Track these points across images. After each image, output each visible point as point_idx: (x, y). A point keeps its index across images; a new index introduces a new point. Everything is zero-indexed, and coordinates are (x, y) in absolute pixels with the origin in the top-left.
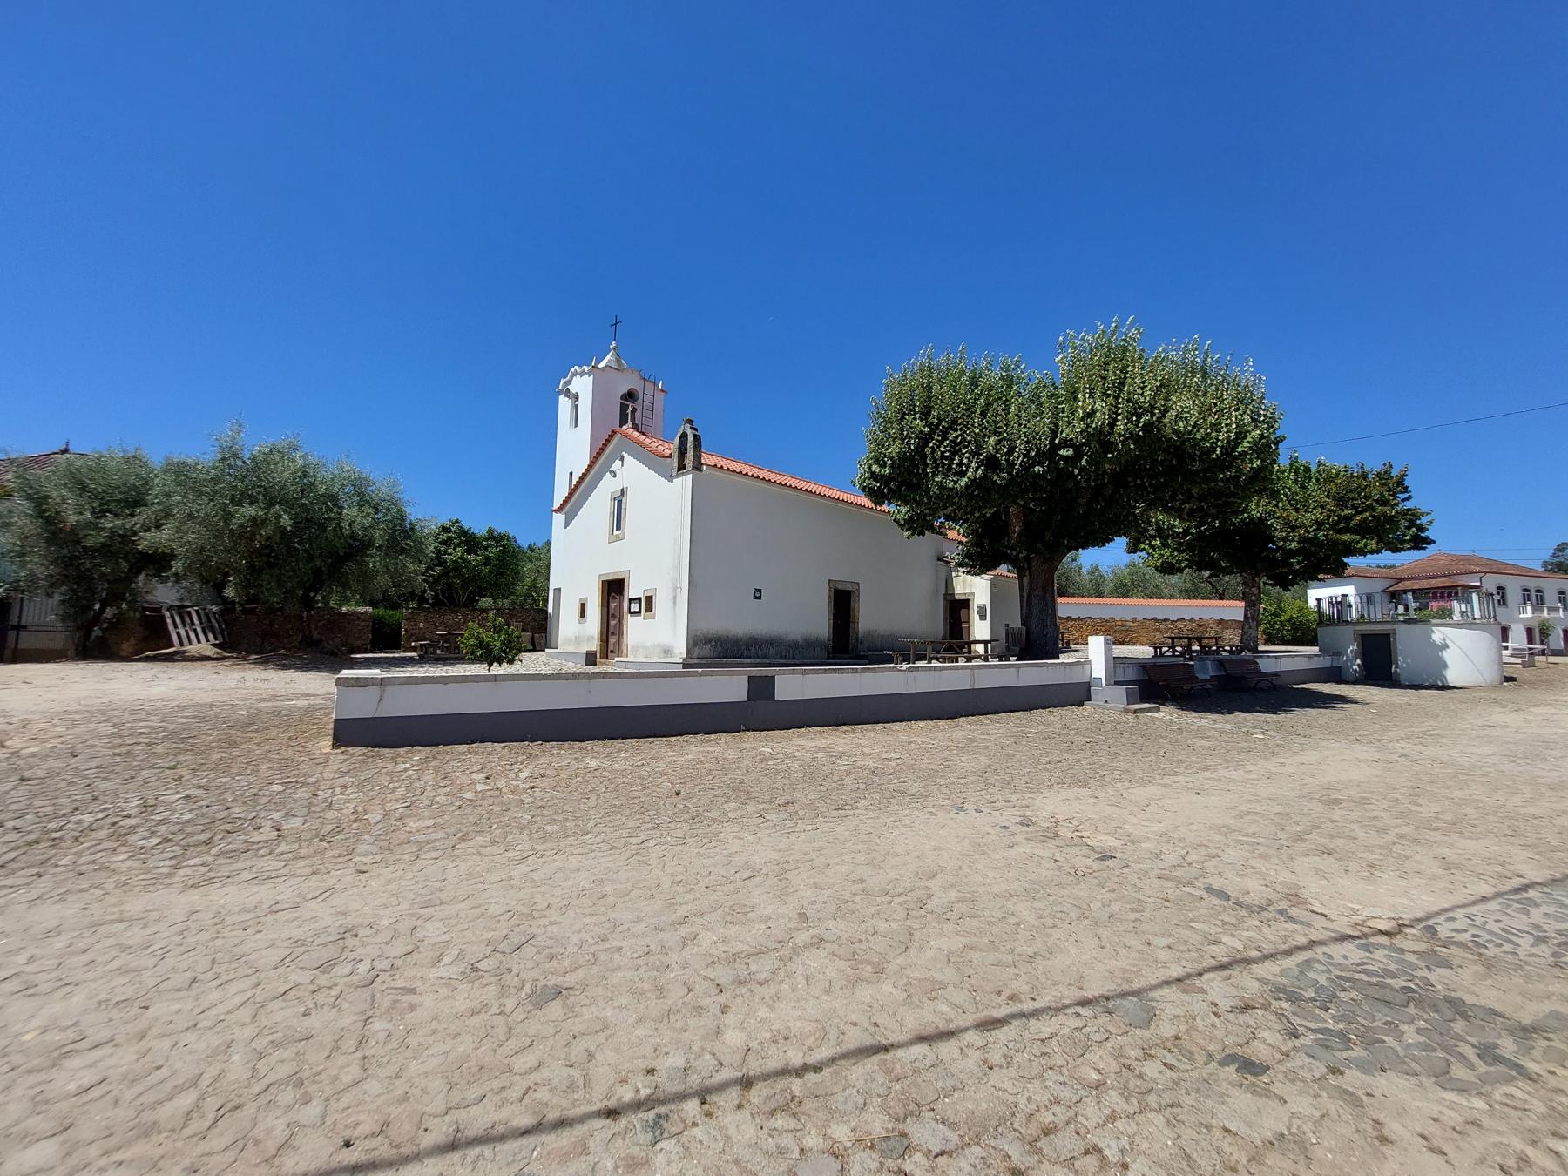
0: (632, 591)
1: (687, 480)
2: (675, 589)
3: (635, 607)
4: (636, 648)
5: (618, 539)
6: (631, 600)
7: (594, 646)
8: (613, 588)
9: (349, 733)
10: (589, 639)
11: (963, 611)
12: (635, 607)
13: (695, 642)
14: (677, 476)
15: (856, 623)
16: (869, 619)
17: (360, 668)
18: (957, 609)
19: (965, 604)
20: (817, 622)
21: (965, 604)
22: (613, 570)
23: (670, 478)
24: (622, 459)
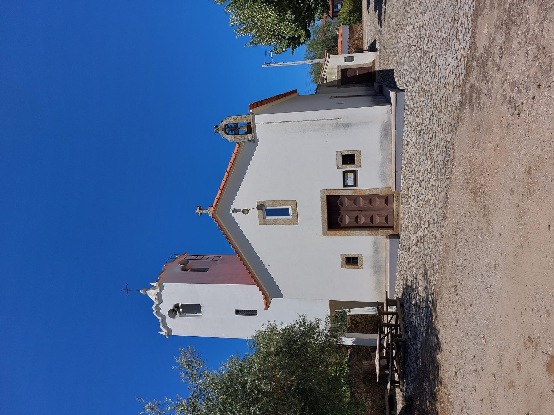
0: (335, 185)
3: (350, 182)
4: (384, 176)
5: (295, 210)
6: (345, 185)
8: (338, 214)
10: (376, 250)
11: (349, 74)
12: (350, 182)
14: (255, 136)
19: (344, 71)
23: (255, 141)
24: (236, 211)
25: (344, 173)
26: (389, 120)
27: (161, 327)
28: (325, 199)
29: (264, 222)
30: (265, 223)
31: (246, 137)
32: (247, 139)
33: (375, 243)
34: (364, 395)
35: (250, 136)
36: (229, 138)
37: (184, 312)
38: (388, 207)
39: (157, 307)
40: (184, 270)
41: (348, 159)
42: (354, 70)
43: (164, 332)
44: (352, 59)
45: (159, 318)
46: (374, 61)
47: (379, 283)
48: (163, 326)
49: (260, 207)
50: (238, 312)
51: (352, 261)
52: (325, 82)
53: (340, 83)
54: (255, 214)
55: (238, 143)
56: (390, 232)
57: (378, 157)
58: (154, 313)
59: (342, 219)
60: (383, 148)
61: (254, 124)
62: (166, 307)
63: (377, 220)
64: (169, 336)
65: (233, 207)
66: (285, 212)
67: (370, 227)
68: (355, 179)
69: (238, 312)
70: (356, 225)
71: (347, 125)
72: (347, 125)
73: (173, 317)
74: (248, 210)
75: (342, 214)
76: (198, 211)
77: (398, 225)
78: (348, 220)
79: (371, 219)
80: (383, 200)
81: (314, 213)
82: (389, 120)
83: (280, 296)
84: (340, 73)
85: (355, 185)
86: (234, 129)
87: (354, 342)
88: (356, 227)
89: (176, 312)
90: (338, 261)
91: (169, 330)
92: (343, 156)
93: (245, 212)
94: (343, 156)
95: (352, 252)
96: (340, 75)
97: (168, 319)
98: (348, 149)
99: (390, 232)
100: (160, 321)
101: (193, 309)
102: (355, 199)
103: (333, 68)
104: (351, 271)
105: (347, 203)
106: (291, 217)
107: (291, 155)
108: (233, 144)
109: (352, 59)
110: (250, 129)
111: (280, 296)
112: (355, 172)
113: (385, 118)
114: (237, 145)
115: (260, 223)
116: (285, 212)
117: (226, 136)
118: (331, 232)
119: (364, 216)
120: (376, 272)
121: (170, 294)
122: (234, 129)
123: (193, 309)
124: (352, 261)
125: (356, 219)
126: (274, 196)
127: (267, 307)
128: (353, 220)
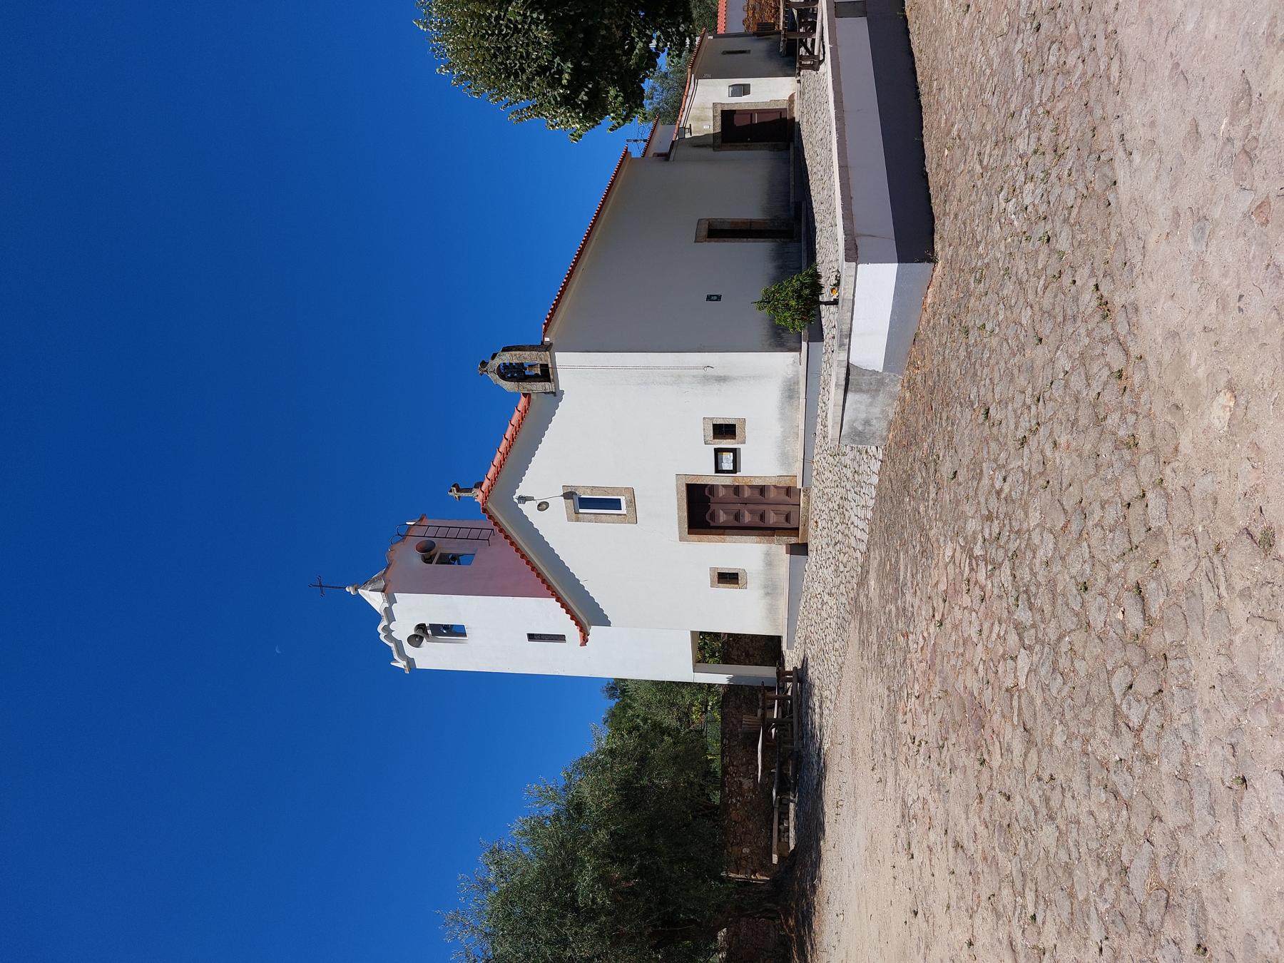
0: (702, 468)
1: (564, 361)
2: (706, 380)
3: (727, 464)
4: (785, 458)
5: (632, 503)
6: (718, 470)
7: (778, 549)
8: (704, 510)
9: (914, 237)
10: (769, 563)
11: (739, 122)
12: (727, 464)
13: (780, 339)
14: (557, 386)
15: (751, 222)
16: (751, 208)
17: (844, 208)
18: (738, 130)
19: (727, 116)
20: (758, 253)
21: (727, 116)
22: (672, 509)
23: (556, 395)
24: (523, 499)
25: (718, 452)
26: (797, 375)
27: (396, 657)
28: (684, 489)
29: (576, 517)
30: (578, 520)
31: (538, 387)
32: (541, 390)
33: (767, 554)
34: (743, 769)
35: (548, 386)
36: (509, 386)
37: (434, 634)
38: (793, 500)
39: (386, 629)
40: (428, 560)
41: (724, 430)
42: (750, 113)
43: (401, 664)
44: (745, 90)
45: (392, 645)
46: (792, 96)
47: (772, 610)
48: (399, 654)
49: (568, 495)
50: (532, 637)
51: (728, 578)
52: (688, 136)
53: (719, 141)
54: (560, 506)
55: (525, 395)
56: (793, 540)
57: (776, 430)
58: (382, 637)
59: (713, 516)
60: (784, 417)
61: (555, 368)
62: (403, 629)
63: (772, 519)
64: (410, 669)
65: (519, 493)
66: (615, 504)
67: (761, 529)
68: (735, 462)
69: (532, 637)
70: (736, 524)
71: (722, 379)
72: (722, 379)
73: (418, 646)
74: (547, 504)
75: (713, 507)
76: (454, 493)
77: (806, 531)
78: (722, 518)
79: (762, 517)
80: (783, 491)
81: (667, 509)
82: (797, 375)
83: (605, 622)
84: (719, 118)
85: (735, 470)
86: (515, 373)
87: (730, 680)
88: (737, 528)
89: (422, 638)
90: (706, 578)
91: (411, 662)
92: (715, 426)
93: (543, 506)
94: (715, 426)
95: (728, 566)
96: (719, 123)
97: (409, 650)
98: (725, 415)
99: (793, 540)
100: (394, 649)
101: (454, 631)
102: (737, 489)
103: (704, 108)
104: (727, 591)
105: (722, 493)
106: (623, 511)
107: (622, 421)
108: (514, 398)
109: (745, 90)
110: (546, 374)
111: (605, 622)
112: (734, 451)
113: (789, 372)
114: (523, 400)
115: (570, 519)
116: (615, 504)
117: (502, 383)
118: (695, 537)
119: (751, 512)
120: (767, 594)
121: (410, 611)
122: (515, 373)
123: (454, 631)
124: (728, 578)
125: (737, 516)
126: (591, 480)
127: (585, 641)
128: (732, 517)
